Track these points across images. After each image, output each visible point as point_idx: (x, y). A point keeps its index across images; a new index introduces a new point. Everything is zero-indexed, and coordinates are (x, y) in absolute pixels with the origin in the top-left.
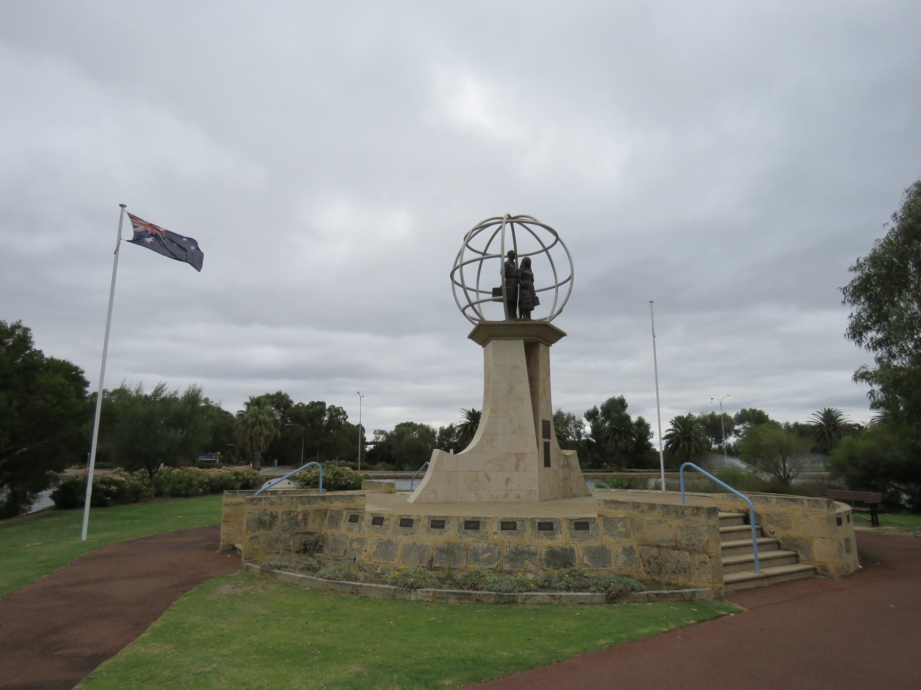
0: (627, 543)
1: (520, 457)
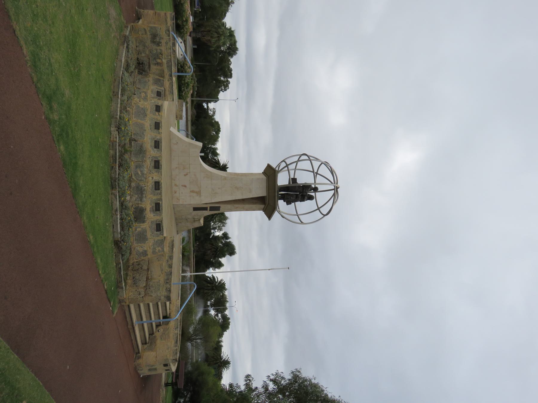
0: (150, 252)
1: (199, 193)
